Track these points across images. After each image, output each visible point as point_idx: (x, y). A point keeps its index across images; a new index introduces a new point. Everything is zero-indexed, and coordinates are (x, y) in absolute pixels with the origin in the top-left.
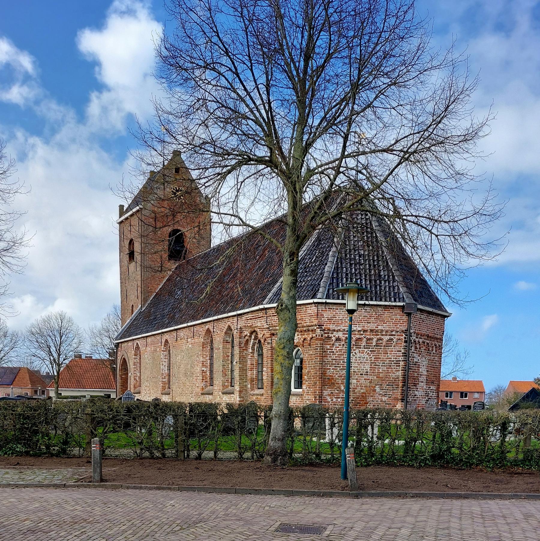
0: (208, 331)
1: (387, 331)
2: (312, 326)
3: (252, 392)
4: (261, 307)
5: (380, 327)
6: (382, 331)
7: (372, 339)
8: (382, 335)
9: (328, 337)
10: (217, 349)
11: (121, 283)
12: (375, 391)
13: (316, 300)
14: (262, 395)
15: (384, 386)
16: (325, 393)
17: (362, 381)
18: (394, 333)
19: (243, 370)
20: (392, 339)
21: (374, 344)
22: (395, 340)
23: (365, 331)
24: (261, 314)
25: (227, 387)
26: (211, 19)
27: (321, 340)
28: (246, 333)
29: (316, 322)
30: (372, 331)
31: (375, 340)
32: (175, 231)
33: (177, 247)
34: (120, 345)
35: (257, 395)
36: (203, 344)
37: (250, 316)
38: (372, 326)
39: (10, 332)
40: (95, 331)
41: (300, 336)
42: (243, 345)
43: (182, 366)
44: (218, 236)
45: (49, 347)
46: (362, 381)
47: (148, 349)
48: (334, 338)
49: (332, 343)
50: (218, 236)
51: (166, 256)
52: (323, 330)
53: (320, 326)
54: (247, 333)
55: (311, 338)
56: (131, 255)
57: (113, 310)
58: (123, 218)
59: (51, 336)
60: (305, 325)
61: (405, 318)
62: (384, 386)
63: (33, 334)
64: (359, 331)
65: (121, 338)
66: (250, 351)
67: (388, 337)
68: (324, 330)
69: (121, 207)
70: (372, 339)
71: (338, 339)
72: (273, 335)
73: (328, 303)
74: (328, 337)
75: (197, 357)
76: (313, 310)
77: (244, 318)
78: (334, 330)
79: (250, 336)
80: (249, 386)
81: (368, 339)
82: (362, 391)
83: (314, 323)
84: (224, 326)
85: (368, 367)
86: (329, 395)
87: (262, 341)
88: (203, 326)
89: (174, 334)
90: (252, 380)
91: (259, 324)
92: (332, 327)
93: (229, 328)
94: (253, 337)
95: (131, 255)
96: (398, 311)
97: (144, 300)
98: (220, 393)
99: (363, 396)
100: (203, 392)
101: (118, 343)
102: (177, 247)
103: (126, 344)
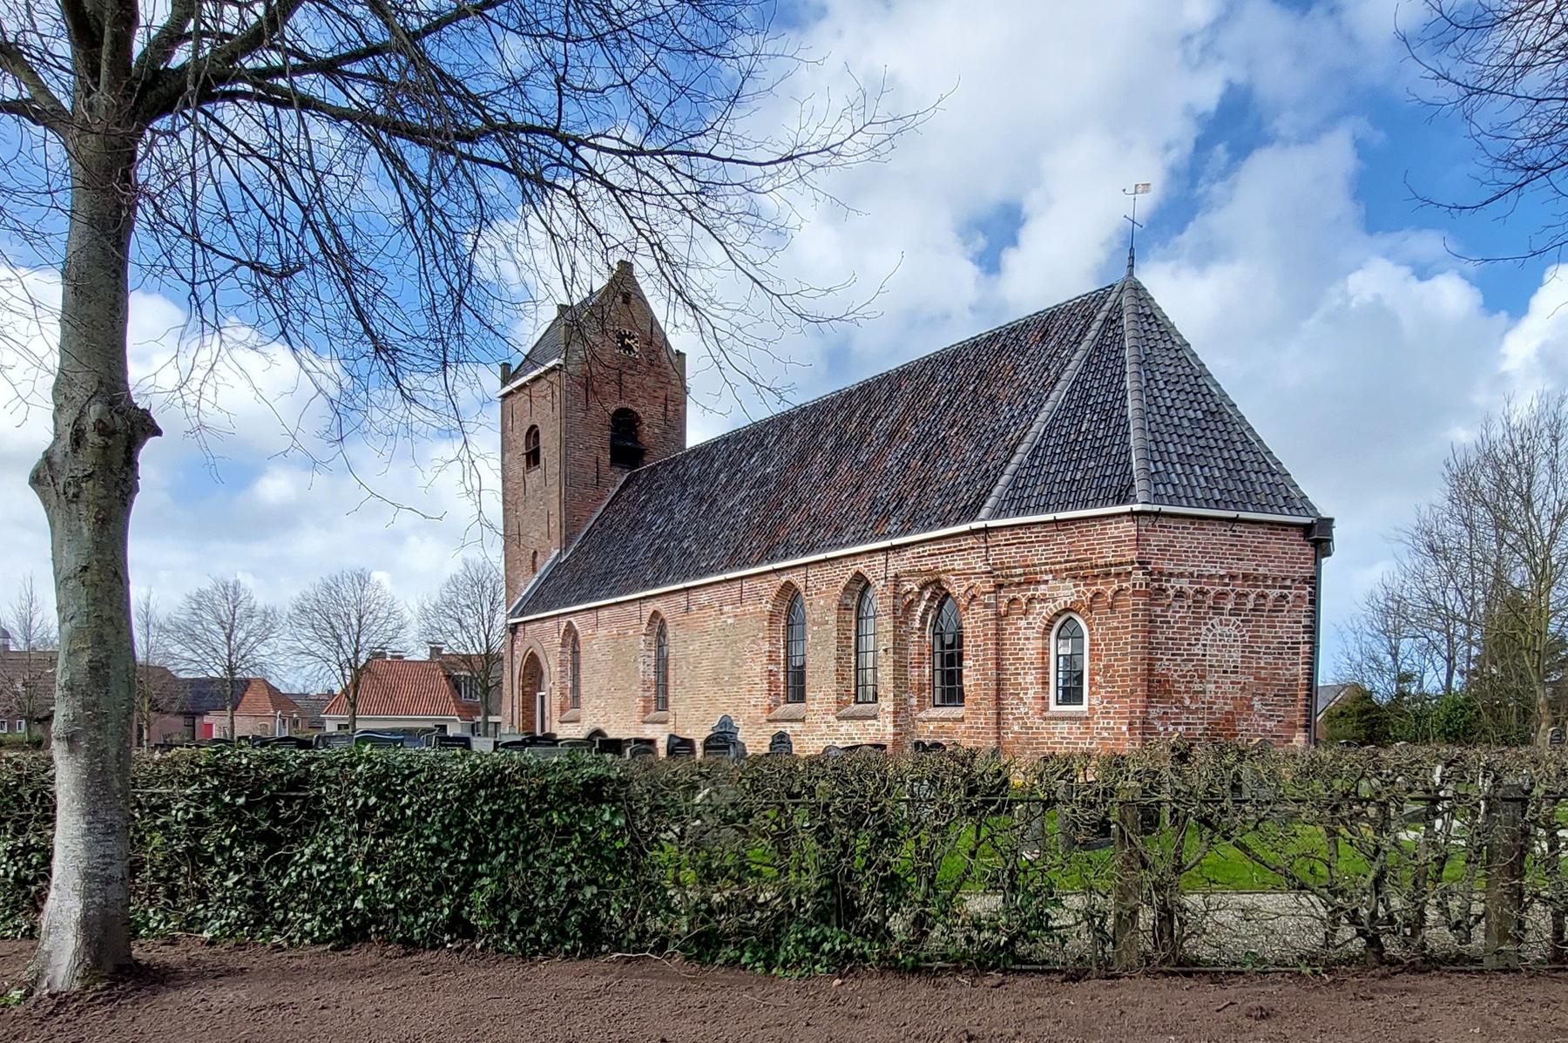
0: (788, 586)
1: (1274, 579)
2: (1121, 564)
3: (922, 715)
4: (976, 525)
5: (1261, 570)
6: (1266, 577)
7: (1246, 595)
8: (1267, 587)
9: (1160, 589)
10: (815, 623)
11: (505, 510)
12: (1250, 707)
13: (1137, 507)
14: (962, 719)
15: (1269, 697)
16: (1153, 713)
17: (1227, 687)
18: (1288, 583)
19: (900, 667)
20: (1284, 597)
21: (1250, 605)
22: (1290, 598)
23: (1233, 577)
24: (971, 541)
25: (847, 703)
26: (366, 338)
27: (1145, 594)
28: (908, 587)
29: (1133, 556)
30: (1246, 577)
31: (1252, 596)
32: (621, 412)
33: (626, 442)
34: (521, 627)
35: (943, 720)
36: (772, 615)
37: (933, 548)
38: (1240, 568)
39: (260, 605)
40: (427, 606)
41: (1082, 588)
42: (899, 613)
43: (705, 663)
44: (698, 431)
45: (338, 638)
46: (1227, 687)
47: (602, 632)
48: (1171, 592)
49: (1166, 602)
50: (698, 431)
51: (606, 458)
52: (1150, 574)
53: (1143, 564)
54: (912, 585)
55: (1116, 593)
56: (533, 457)
57: (462, 567)
58: (508, 389)
59: (336, 614)
60: (1100, 562)
61: (1309, 550)
62: (1269, 697)
63: (303, 611)
64: (1222, 577)
65: (522, 614)
66: (917, 624)
67: (1278, 591)
68: (1150, 574)
69: (506, 367)
70: (1246, 595)
71: (1180, 594)
72: (1000, 586)
73: (1166, 515)
74: (1160, 589)
75: (753, 642)
76: (1128, 528)
77: (909, 554)
78: (1171, 575)
79: (920, 594)
80: (914, 701)
81: (1239, 595)
82: (1227, 708)
83: (1128, 558)
84: (845, 574)
85: (1237, 655)
86: (1160, 718)
87: (963, 602)
88: (773, 577)
89: (682, 599)
90: (921, 689)
91: (958, 565)
92: (1168, 567)
93: (860, 584)
94: (927, 595)
95: (533, 457)
96: (1296, 535)
97: (568, 540)
98: (831, 718)
99: (1227, 720)
100: (771, 716)
101: (516, 624)
102: (626, 442)
103: (537, 625)
